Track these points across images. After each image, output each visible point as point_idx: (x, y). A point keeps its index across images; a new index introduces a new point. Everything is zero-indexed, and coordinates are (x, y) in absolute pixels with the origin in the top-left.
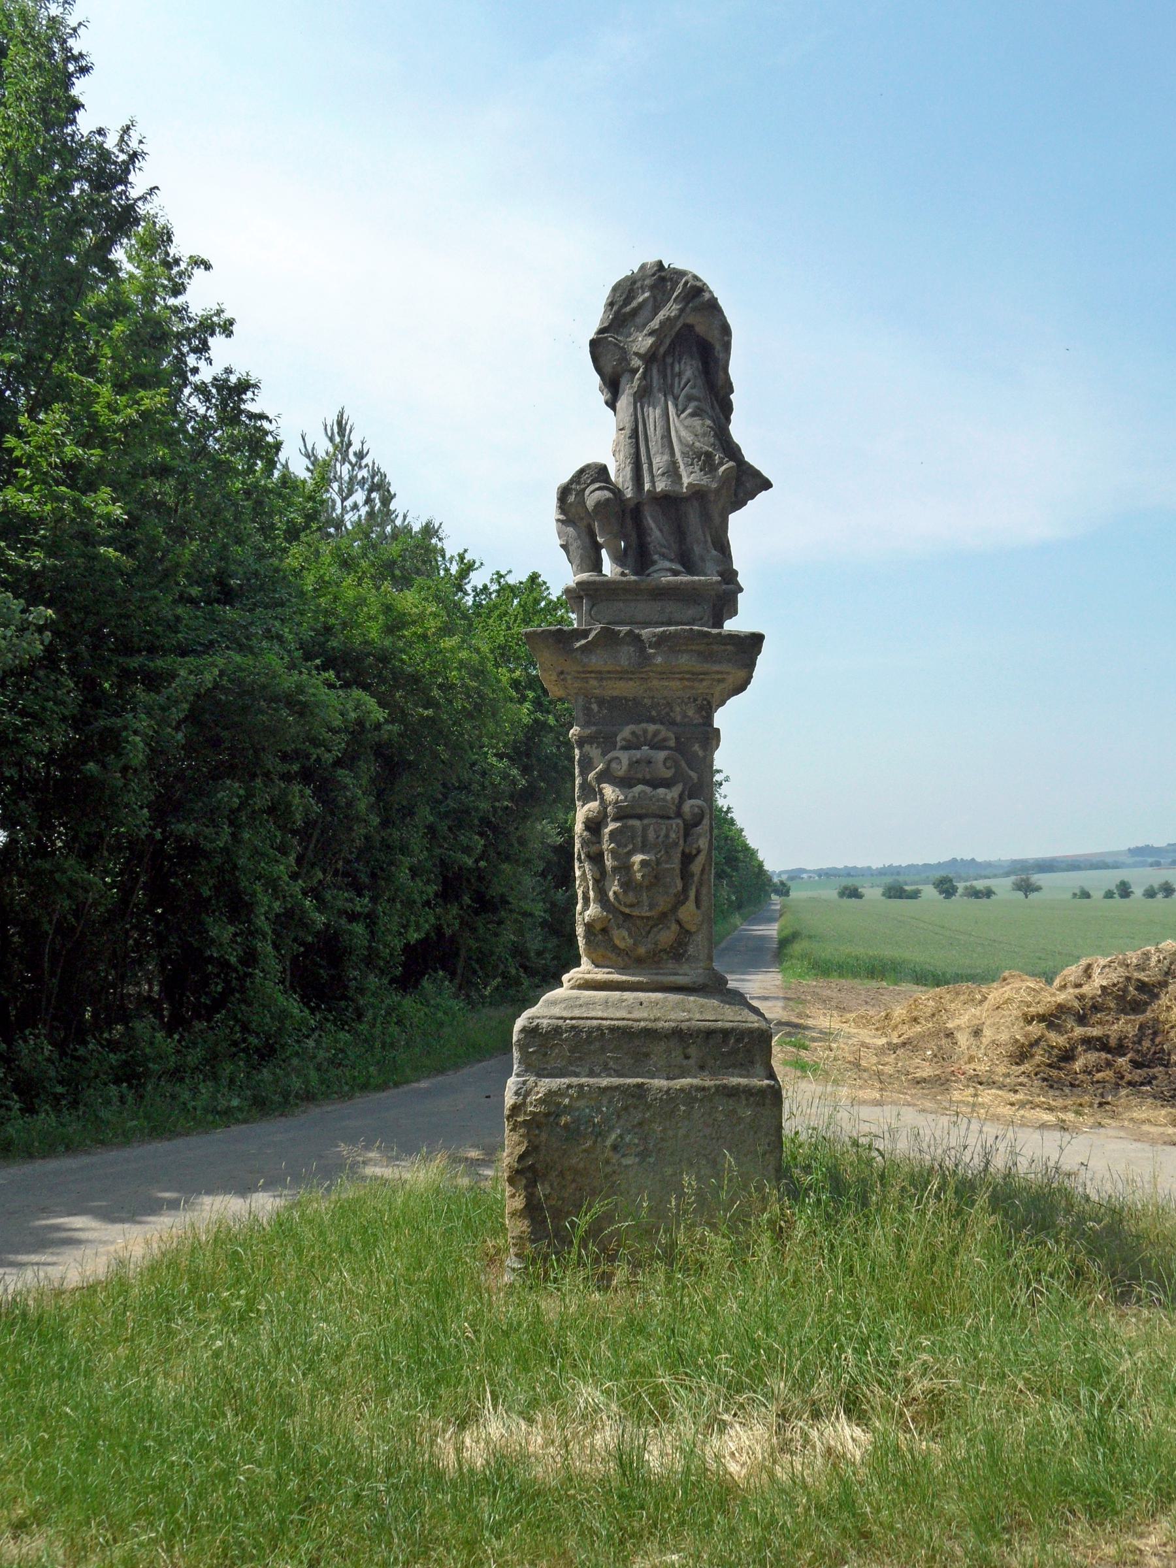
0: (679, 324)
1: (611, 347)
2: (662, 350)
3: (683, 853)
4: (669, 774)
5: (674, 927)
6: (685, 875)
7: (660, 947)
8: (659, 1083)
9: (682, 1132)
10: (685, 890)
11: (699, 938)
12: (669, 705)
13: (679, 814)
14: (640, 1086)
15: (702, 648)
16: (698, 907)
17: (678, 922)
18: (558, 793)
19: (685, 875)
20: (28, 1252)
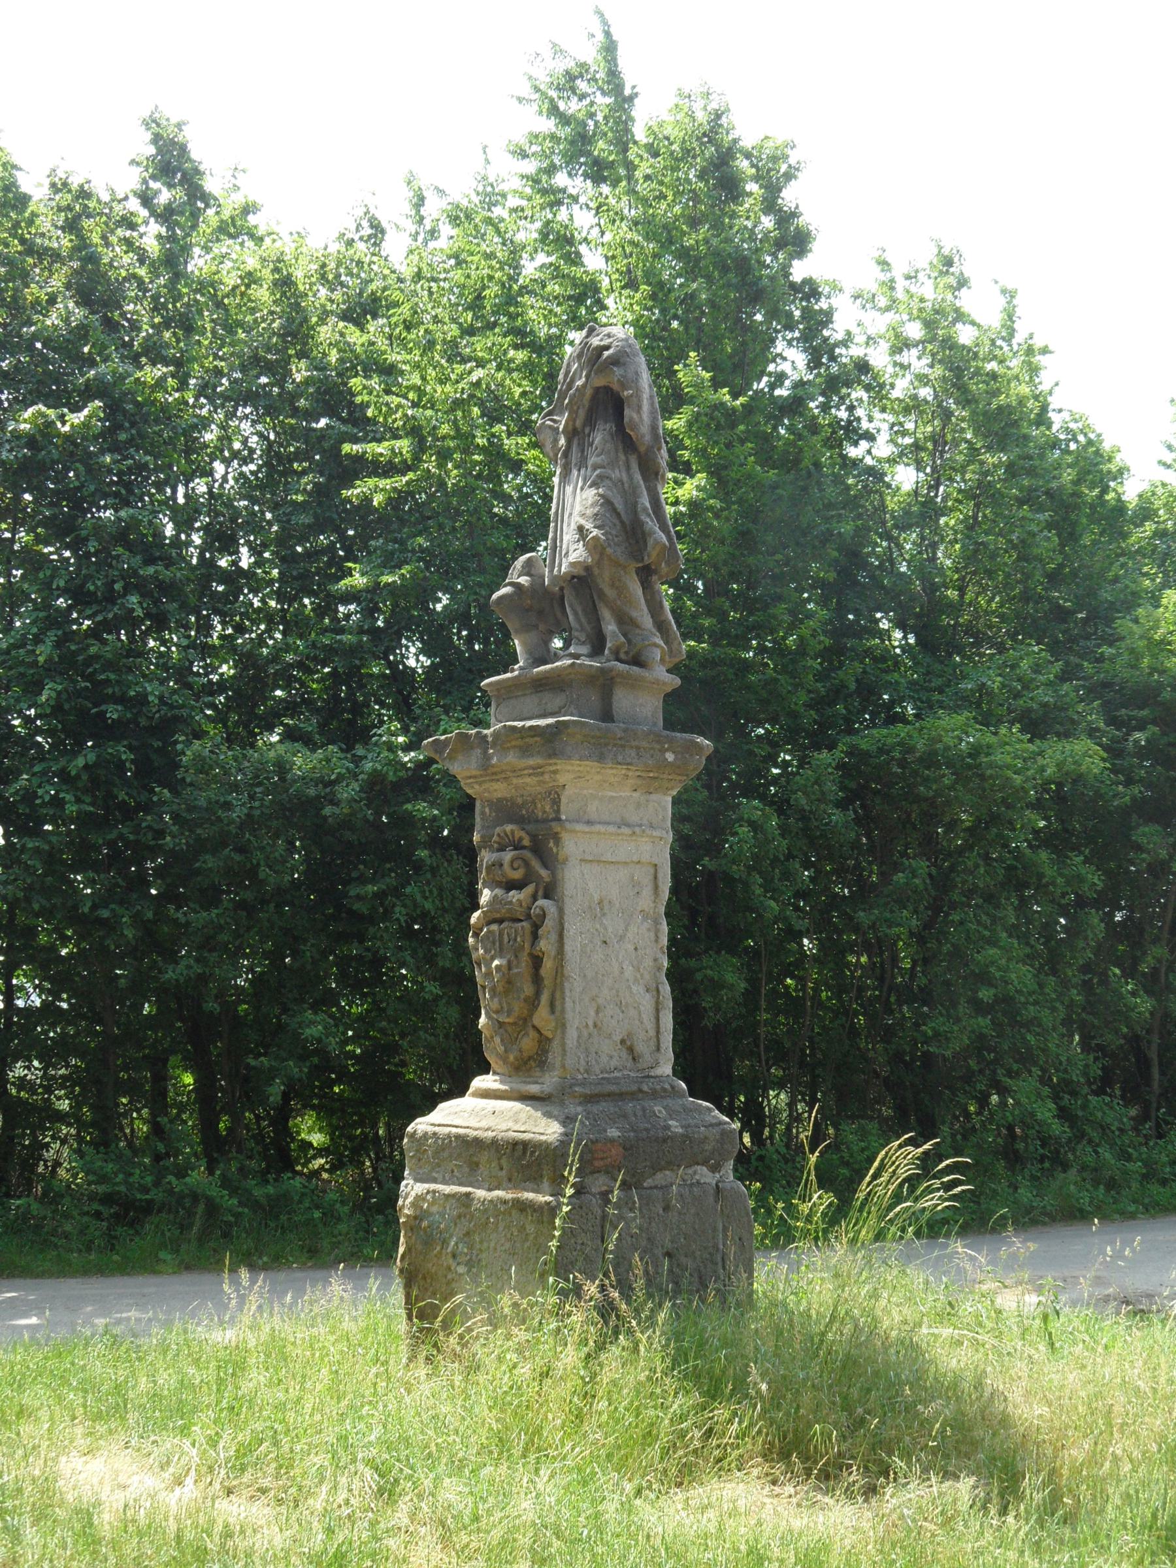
0: (589, 392)
1: (548, 431)
2: (578, 423)
3: (531, 955)
4: (517, 875)
5: (533, 1034)
6: (537, 980)
7: (525, 1055)
8: (481, 1193)
9: (492, 1244)
10: (538, 994)
11: (555, 1044)
12: (533, 802)
13: (529, 917)
14: (468, 1195)
15: (519, 742)
16: (553, 1011)
17: (534, 1027)
18: (1039, 847)
19: (537, 980)
20: (21, 1317)
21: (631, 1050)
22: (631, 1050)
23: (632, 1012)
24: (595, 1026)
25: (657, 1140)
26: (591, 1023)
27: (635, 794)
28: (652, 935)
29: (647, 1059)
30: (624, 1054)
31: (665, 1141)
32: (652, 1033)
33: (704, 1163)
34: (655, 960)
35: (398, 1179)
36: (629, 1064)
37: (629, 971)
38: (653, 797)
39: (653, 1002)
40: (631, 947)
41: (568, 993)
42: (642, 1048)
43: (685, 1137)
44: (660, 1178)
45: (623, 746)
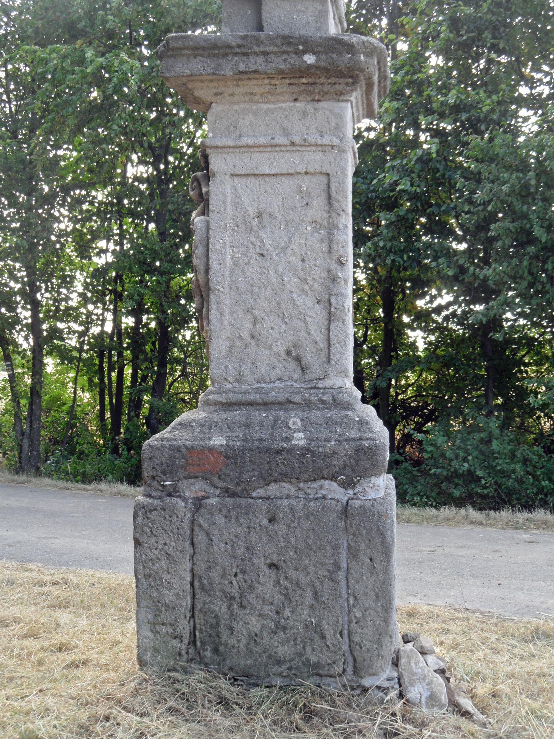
21: (298, 360)
22: (298, 360)
23: (297, 323)
24: (253, 337)
25: (268, 450)
26: (245, 334)
27: (298, 104)
28: (325, 247)
29: (316, 370)
30: (292, 365)
31: (279, 452)
32: (323, 344)
33: (333, 478)
34: (329, 271)
35: (211, 449)
36: (297, 374)
37: (292, 283)
38: (321, 104)
39: (325, 313)
40: (296, 260)
41: (213, 306)
42: (308, 358)
43: (306, 450)
44: (273, 489)
45: (246, 54)
